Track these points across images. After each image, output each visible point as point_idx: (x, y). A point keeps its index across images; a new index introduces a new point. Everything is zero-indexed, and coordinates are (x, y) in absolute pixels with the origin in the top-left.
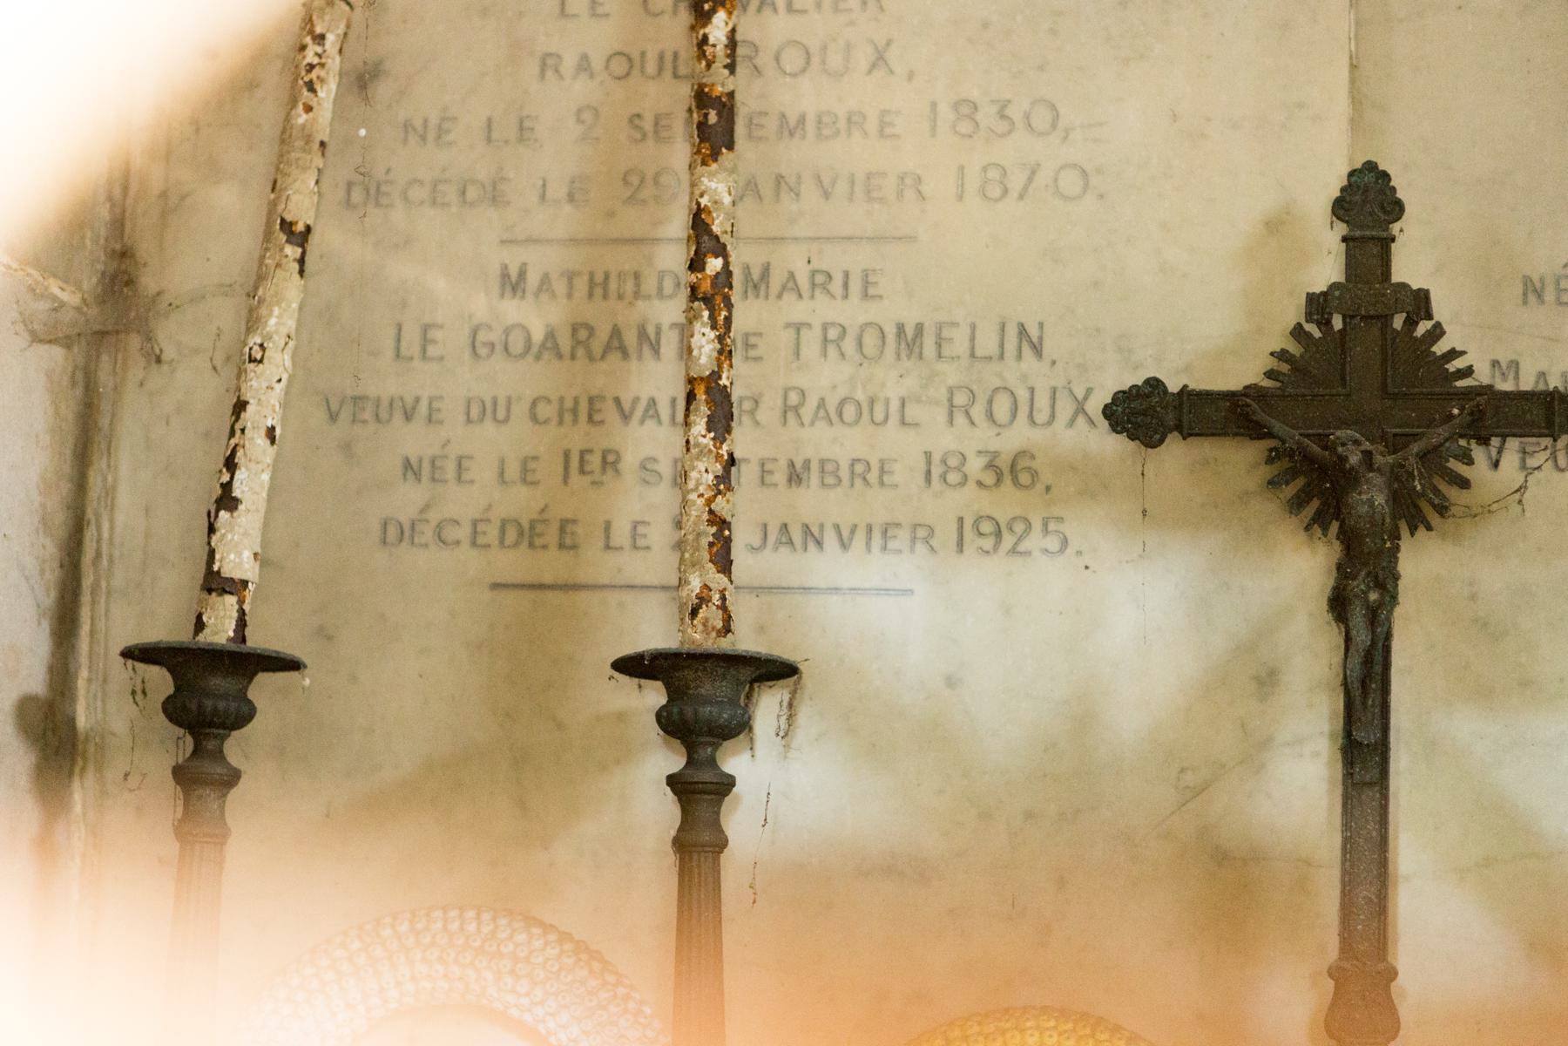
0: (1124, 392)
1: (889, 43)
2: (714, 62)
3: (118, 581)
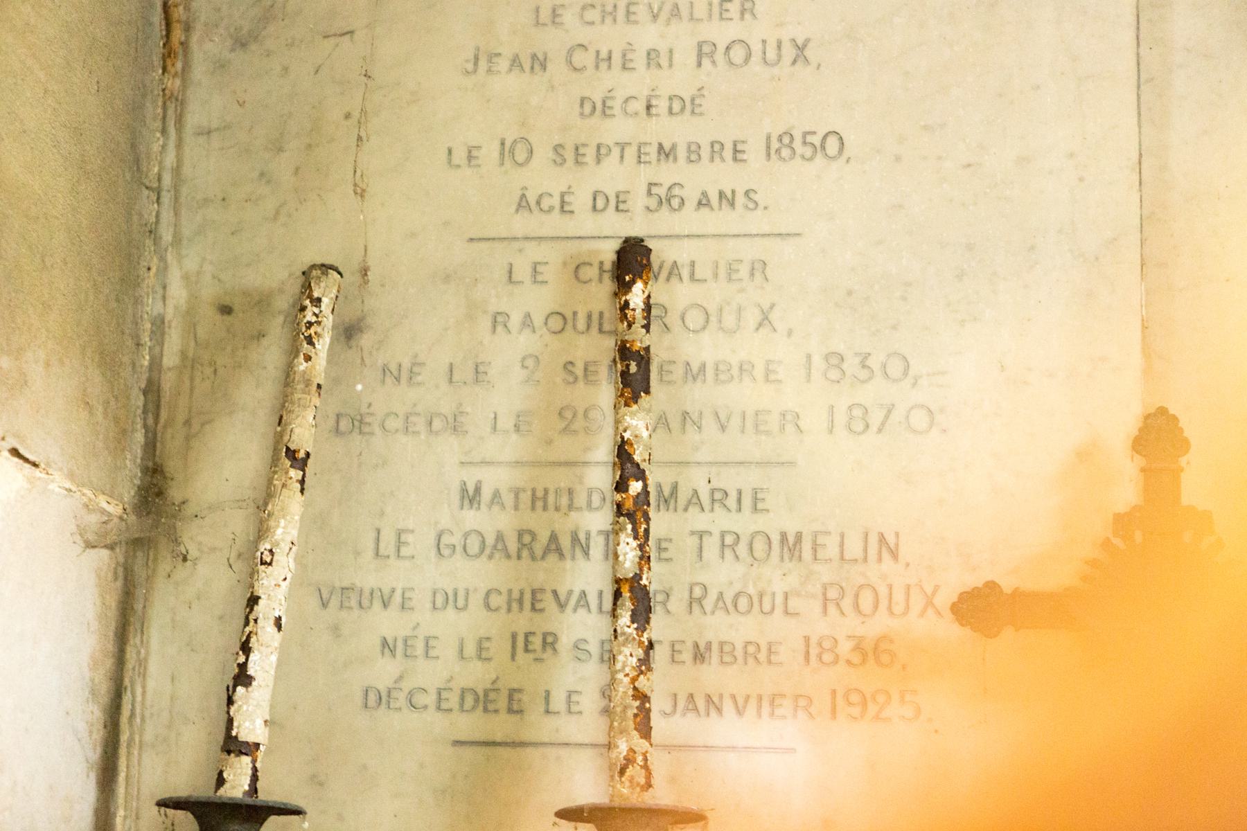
1: (772, 306)
2: (634, 323)
3: (149, 736)
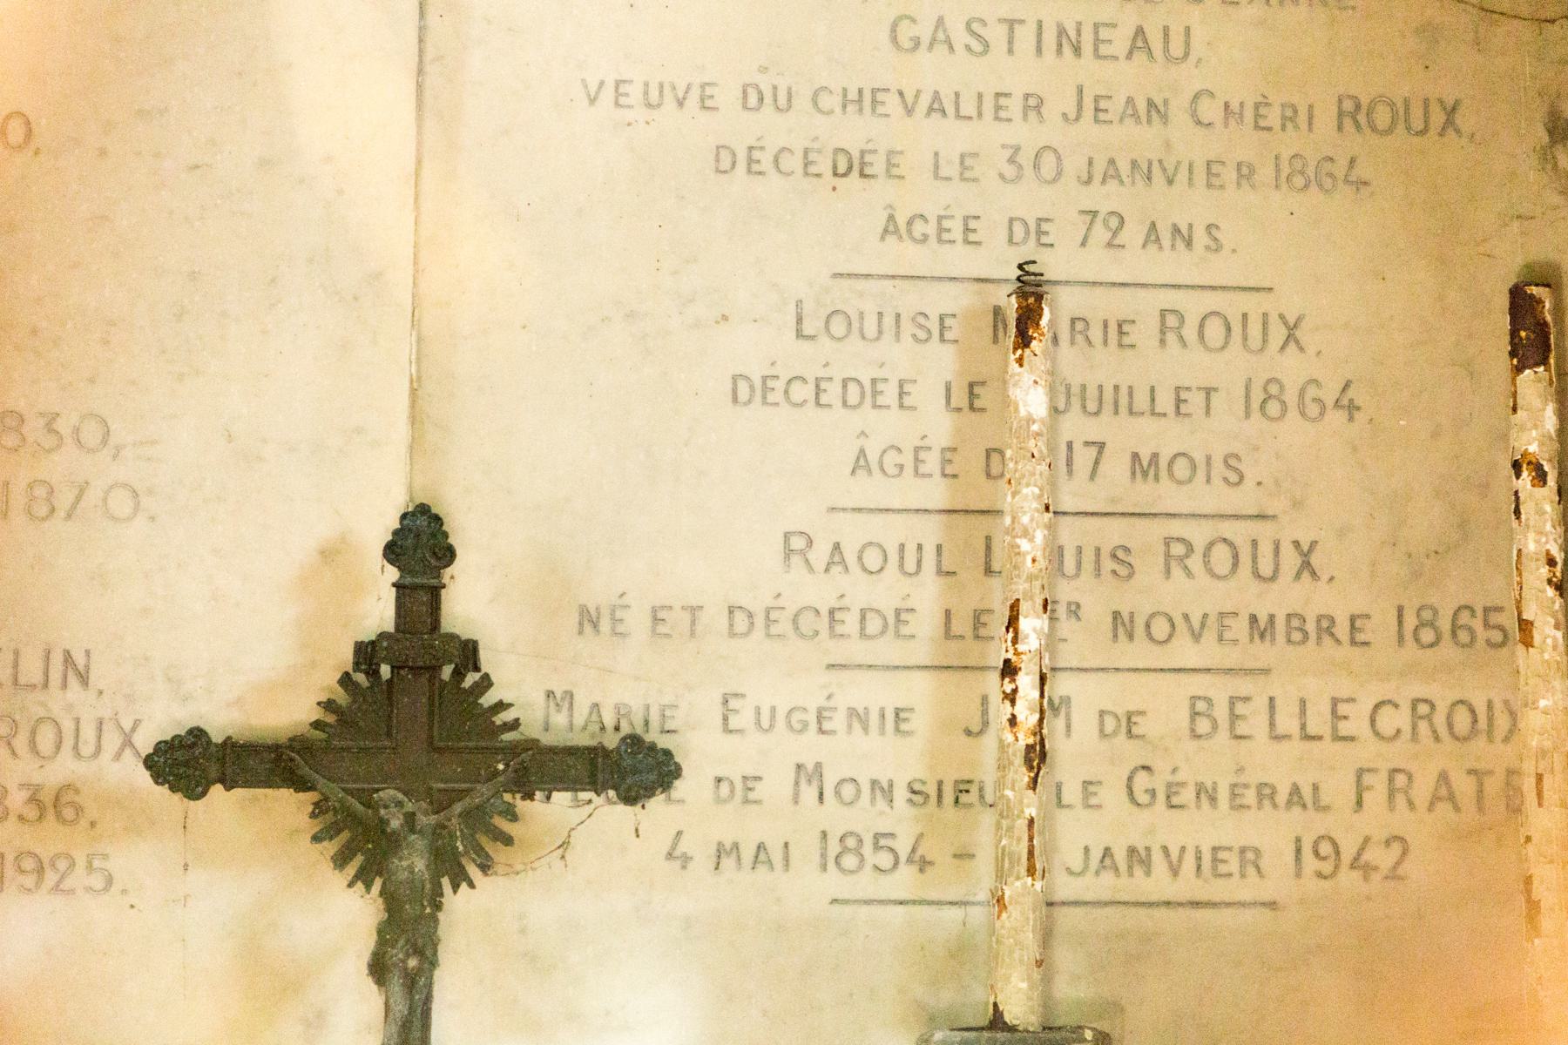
0: (166, 742)
